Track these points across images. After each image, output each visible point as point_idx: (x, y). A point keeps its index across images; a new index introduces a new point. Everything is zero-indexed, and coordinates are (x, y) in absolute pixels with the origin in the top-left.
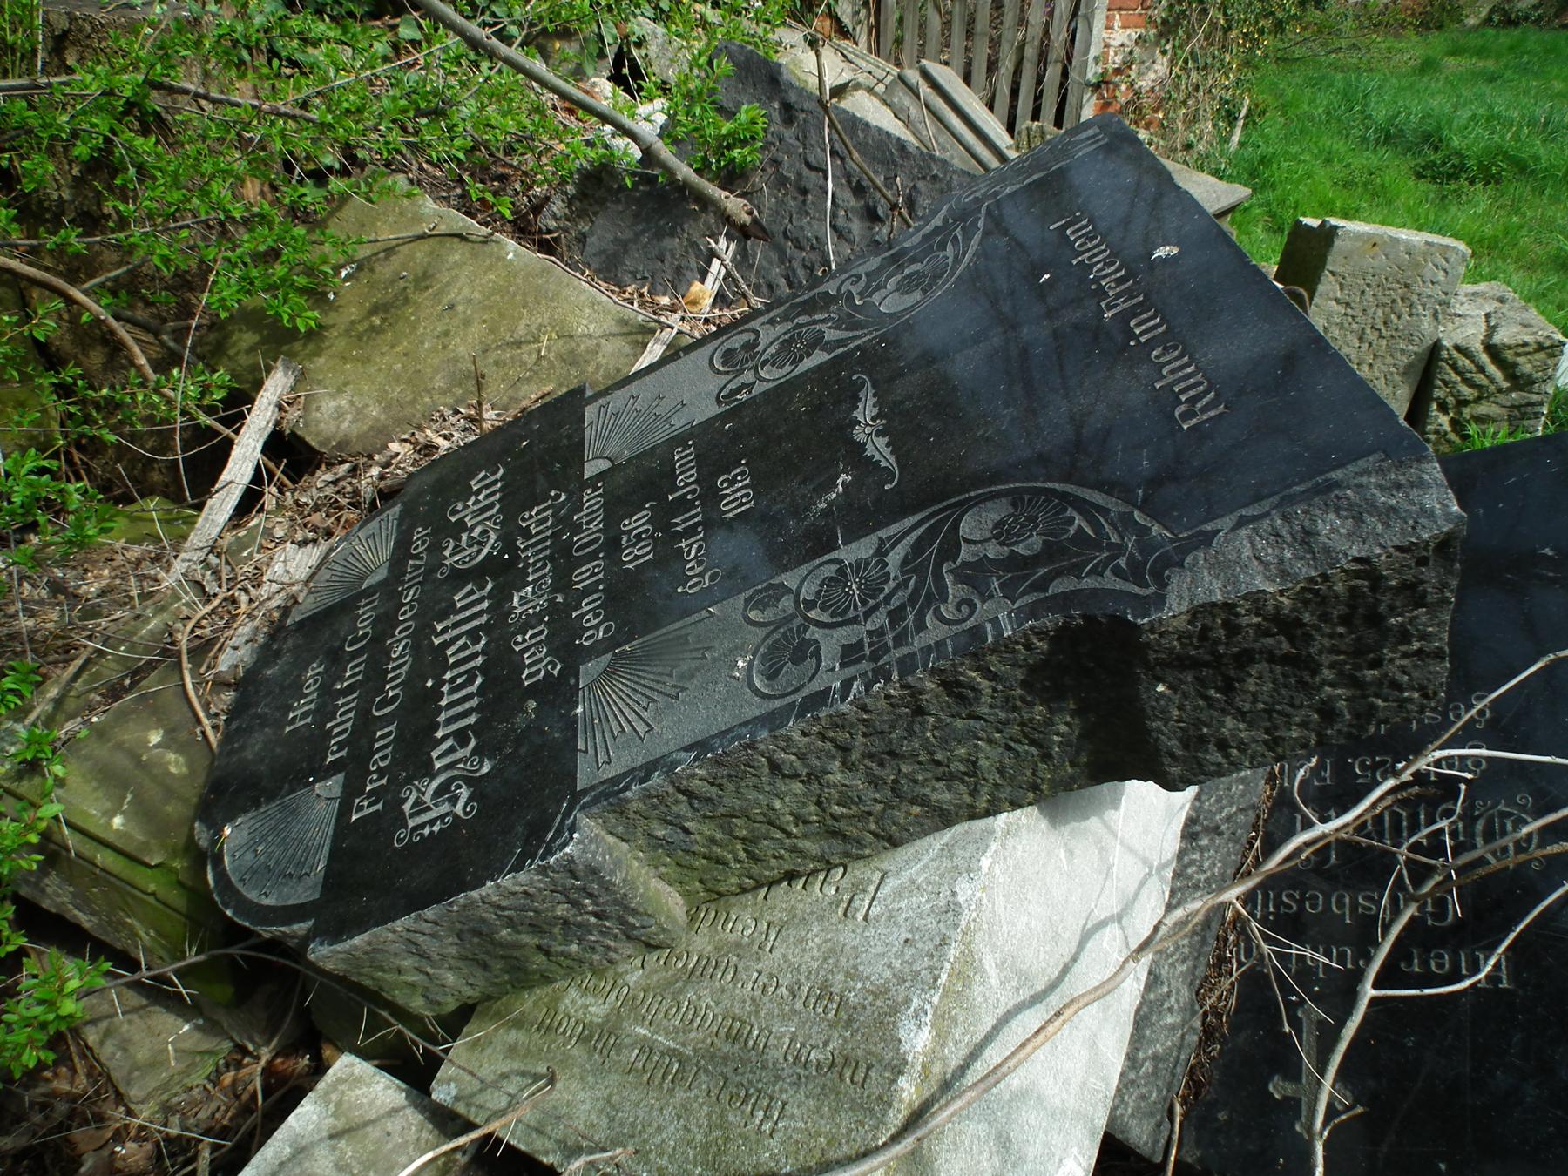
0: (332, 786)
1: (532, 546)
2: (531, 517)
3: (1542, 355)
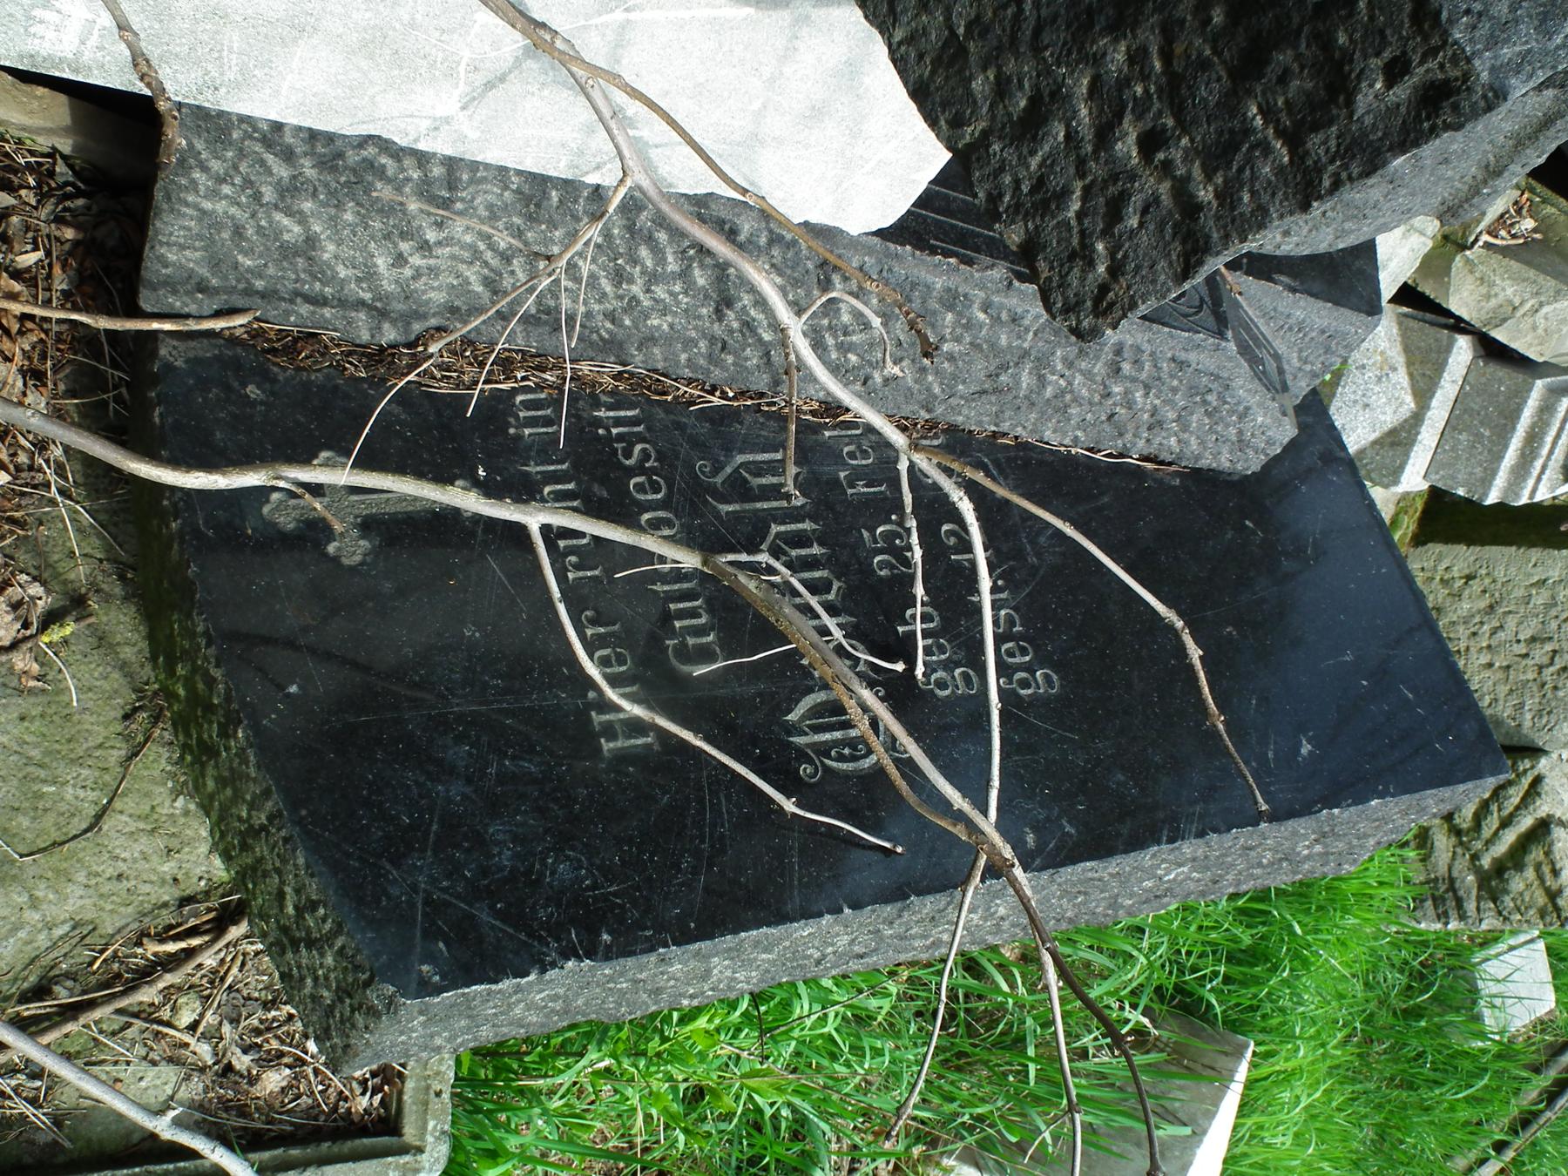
3: (1541, 899)
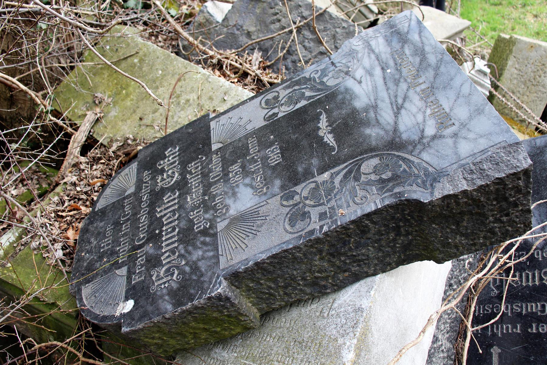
0: (124, 271)
1: (193, 177)
2: (192, 166)
